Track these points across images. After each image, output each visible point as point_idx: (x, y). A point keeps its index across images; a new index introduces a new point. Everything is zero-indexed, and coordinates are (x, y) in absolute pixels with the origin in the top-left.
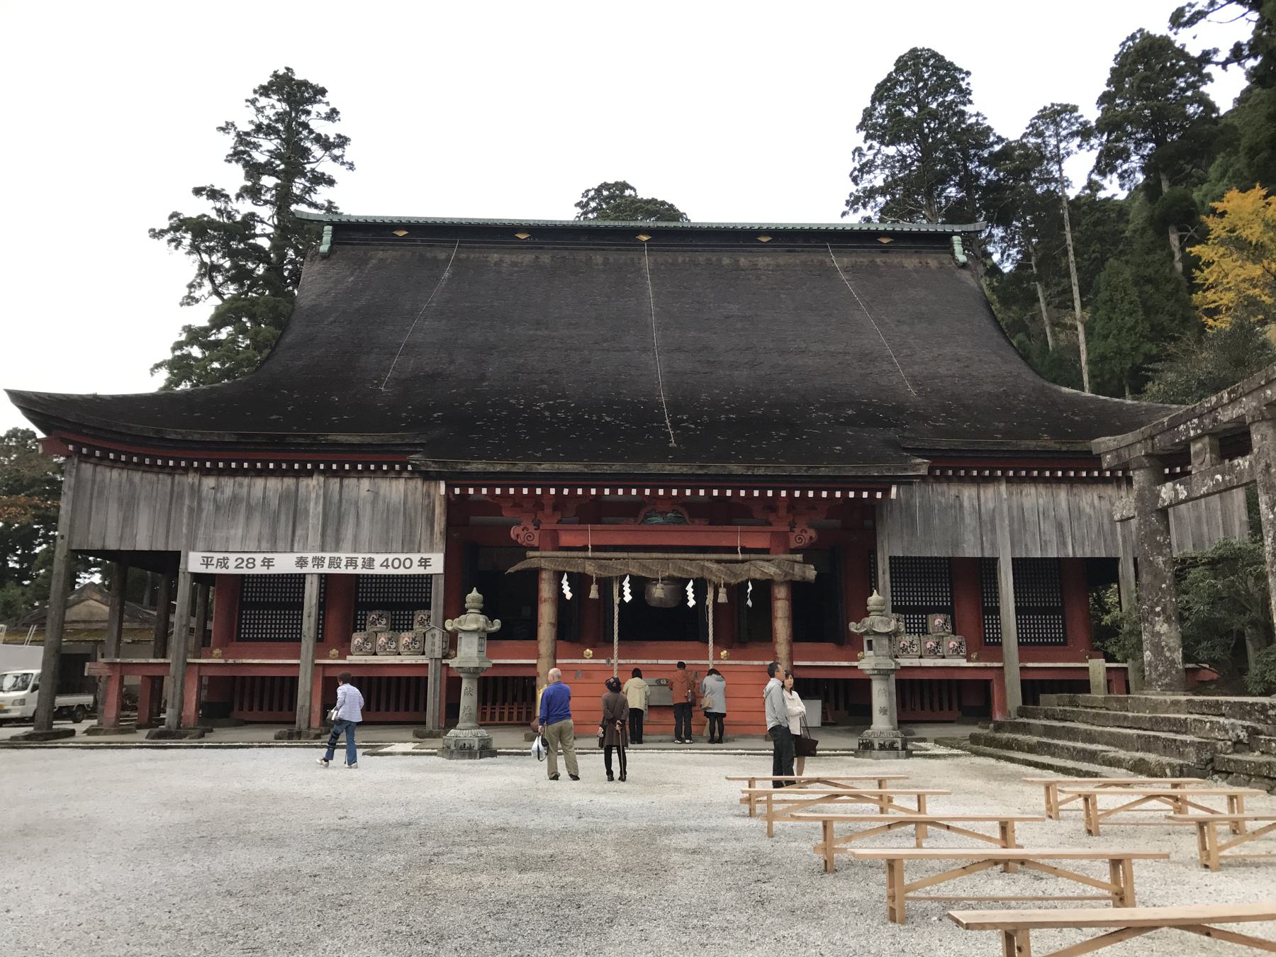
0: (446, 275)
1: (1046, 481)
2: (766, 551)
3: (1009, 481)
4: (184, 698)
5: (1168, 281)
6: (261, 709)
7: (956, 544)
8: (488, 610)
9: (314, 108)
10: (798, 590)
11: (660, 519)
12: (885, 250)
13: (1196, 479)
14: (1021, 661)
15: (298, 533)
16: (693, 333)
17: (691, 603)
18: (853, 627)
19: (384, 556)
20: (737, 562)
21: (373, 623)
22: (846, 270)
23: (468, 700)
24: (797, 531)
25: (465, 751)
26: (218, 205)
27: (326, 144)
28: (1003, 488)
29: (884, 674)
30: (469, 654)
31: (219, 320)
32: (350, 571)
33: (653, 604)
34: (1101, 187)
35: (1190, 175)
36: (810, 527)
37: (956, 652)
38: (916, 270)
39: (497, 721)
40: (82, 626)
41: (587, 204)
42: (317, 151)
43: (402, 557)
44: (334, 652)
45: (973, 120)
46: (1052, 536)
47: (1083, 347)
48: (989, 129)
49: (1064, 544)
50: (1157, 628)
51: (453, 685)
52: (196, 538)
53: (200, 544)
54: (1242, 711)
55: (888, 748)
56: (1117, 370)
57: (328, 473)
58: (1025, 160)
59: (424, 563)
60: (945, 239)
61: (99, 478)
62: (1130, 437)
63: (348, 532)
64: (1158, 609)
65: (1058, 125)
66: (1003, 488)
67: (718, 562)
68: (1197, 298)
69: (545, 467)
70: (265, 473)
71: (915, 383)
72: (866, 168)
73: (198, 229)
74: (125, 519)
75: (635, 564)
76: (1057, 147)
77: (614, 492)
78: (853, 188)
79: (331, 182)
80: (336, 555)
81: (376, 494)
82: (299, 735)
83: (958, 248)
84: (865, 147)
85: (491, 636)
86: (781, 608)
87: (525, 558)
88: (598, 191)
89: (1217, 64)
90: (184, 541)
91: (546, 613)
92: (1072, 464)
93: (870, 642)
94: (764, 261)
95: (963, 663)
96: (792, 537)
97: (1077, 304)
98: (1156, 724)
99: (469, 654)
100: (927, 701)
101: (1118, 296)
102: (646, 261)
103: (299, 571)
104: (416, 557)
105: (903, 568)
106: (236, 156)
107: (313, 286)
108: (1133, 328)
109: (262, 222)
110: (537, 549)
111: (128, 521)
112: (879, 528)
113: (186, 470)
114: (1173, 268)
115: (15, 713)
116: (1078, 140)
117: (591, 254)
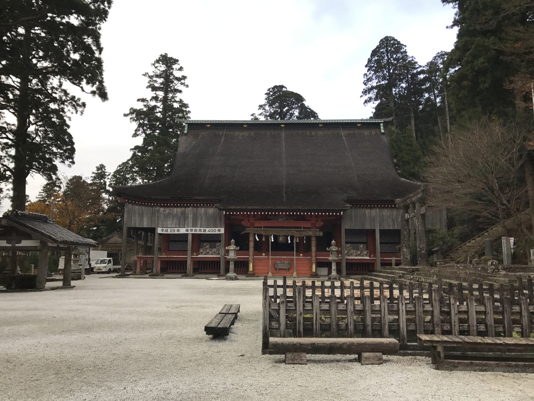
2: (310, 228)
3: (379, 208)
4: (157, 267)
8: (236, 244)
9: (174, 67)
10: (318, 238)
11: (281, 219)
12: (359, 128)
15: (186, 222)
17: (289, 242)
22: (345, 136)
23: (232, 266)
24: (318, 222)
25: (231, 279)
26: (145, 104)
30: (232, 255)
32: (200, 233)
37: (366, 255)
40: (113, 245)
41: (269, 93)
42: (176, 82)
43: (213, 229)
44: (195, 254)
45: (411, 59)
48: (416, 63)
49: (394, 225)
51: (227, 263)
53: (160, 225)
57: (194, 206)
59: (219, 230)
60: (379, 124)
63: (199, 222)
69: (250, 207)
72: (369, 80)
78: (365, 87)
79: (180, 91)
81: (206, 212)
82: (188, 276)
83: (382, 127)
86: (314, 243)
87: (245, 230)
88: (273, 88)
91: (251, 244)
92: (389, 204)
94: (320, 133)
96: (317, 224)
99: (232, 255)
100: (174, 267)
104: (217, 229)
105: (349, 232)
107: (184, 144)
109: (159, 107)
110: (248, 227)
111: (142, 220)
115: (104, 270)
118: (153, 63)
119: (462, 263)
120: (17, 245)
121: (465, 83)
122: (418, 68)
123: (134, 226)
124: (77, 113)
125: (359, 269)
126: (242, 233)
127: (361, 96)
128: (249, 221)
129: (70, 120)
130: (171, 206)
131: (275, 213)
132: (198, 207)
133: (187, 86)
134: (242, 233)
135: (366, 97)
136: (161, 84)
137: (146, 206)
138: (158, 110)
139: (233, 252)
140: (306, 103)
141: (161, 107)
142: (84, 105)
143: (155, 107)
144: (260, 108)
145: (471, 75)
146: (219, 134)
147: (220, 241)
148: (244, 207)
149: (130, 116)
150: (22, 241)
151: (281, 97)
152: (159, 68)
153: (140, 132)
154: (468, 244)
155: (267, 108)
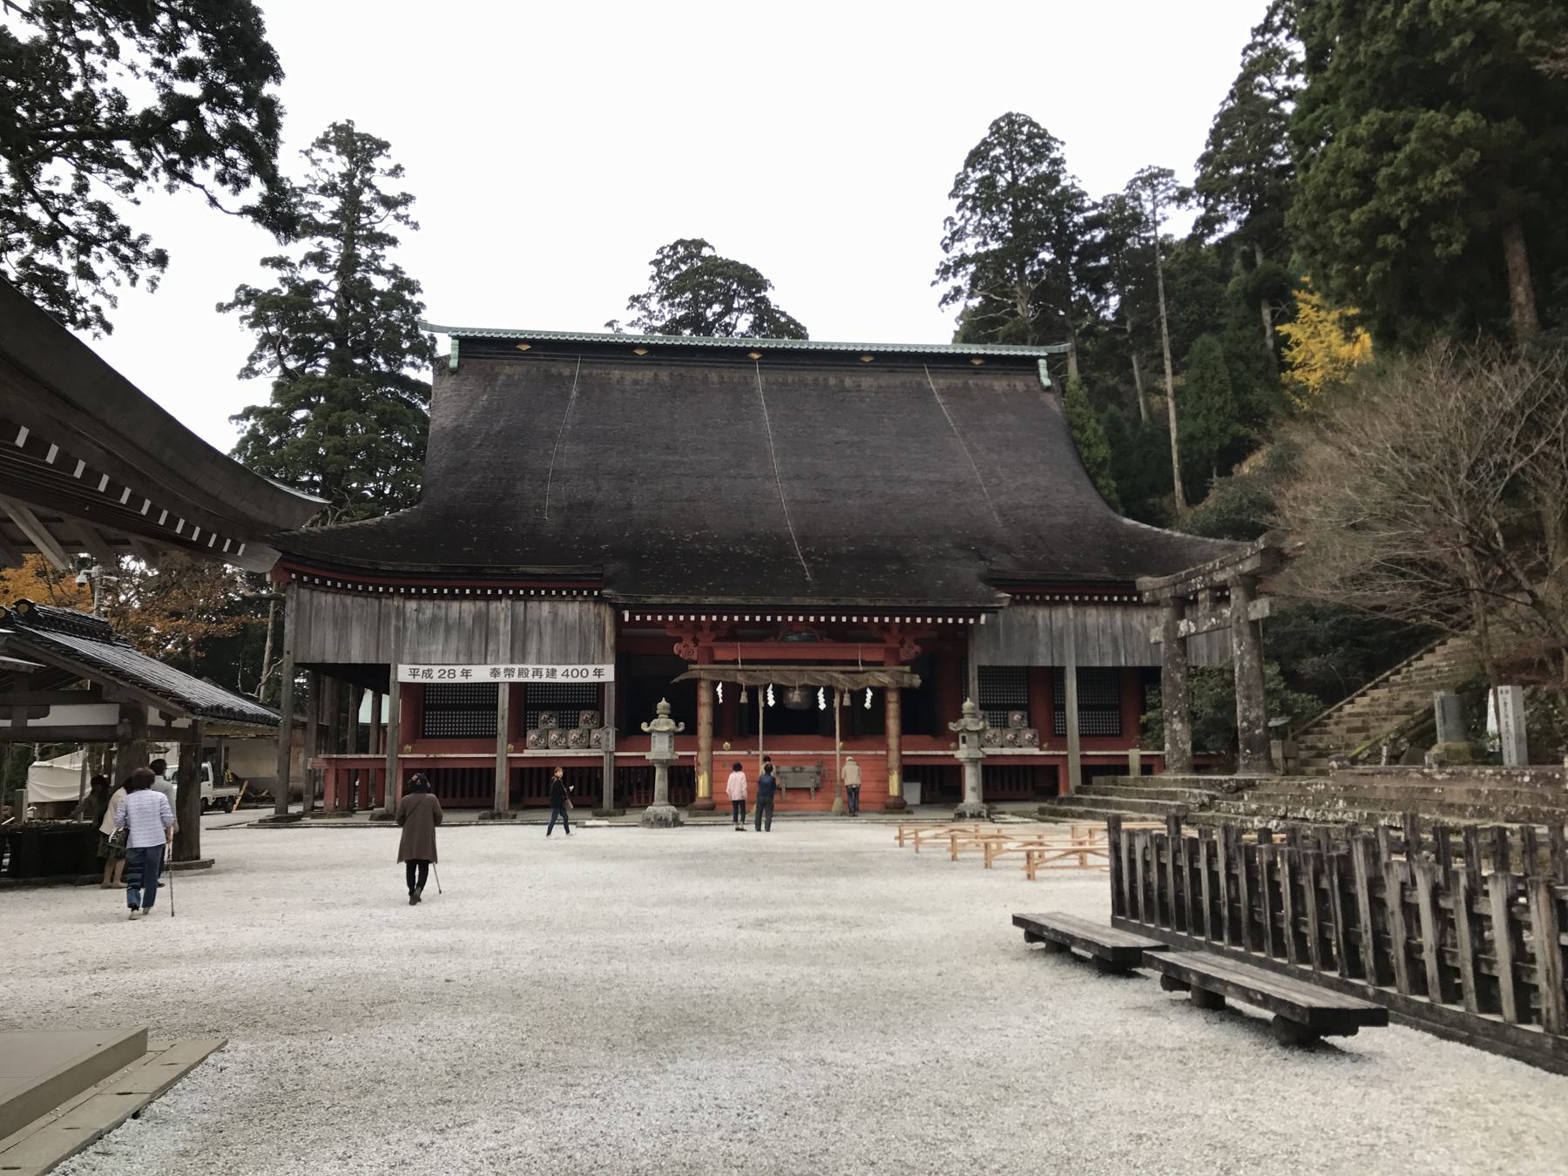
0: (574, 393)
1: (1105, 604)
2: (881, 664)
3: (1075, 604)
5: (1258, 358)
6: (463, 796)
7: (1032, 655)
10: (906, 694)
11: (795, 638)
12: (977, 371)
13: (1201, 621)
14: (1082, 748)
15: (491, 647)
16: (808, 460)
17: (822, 706)
18: (952, 726)
19: (564, 668)
20: (858, 672)
21: (545, 722)
22: (941, 392)
25: (662, 822)
26: (286, 273)
28: (1070, 610)
29: (974, 761)
32: (537, 679)
37: (1031, 743)
38: (1005, 394)
41: (661, 261)
42: (380, 210)
43: (580, 668)
46: (1108, 648)
47: (1173, 425)
48: (1083, 194)
53: (407, 658)
54: (1211, 785)
55: (977, 816)
56: (1205, 451)
58: (1123, 218)
59: (598, 673)
60: (1032, 362)
61: (315, 601)
63: (533, 647)
65: (1153, 187)
66: (1070, 610)
67: (843, 672)
68: (1285, 377)
69: (711, 600)
70: (462, 597)
71: (1001, 513)
72: (958, 235)
74: (340, 637)
75: (777, 675)
76: (1154, 212)
79: (393, 242)
83: (1043, 371)
84: (957, 217)
86: (893, 709)
92: (1121, 593)
94: (867, 382)
95: (1036, 751)
97: (1168, 370)
98: (1159, 795)
101: (1208, 375)
102: (759, 380)
103: (493, 680)
104: (591, 668)
108: (1222, 408)
110: (695, 663)
111: (342, 639)
113: (392, 595)
114: (1264, 345)
117: (706, 371)
118: (308, 147)
119: (1364, 762)
120: (31, 723)
121: (1389, 240)
122: (1088, 209)
123: (318, 660)
124: (133, 283)
126: (676, 680)
127: (934, 283)
128: (696, 641)
129: (114, 306)
130: (441, 596)
131: (763, 619)
132: (530, 598)
133: (416, 226)
134: (676, 680)
135: (946, 287)
136: (335, 215)
137: (357, 594)
138: (323, 296)
139: (666, 738)
140: (775, 297)
141: (335, 286)
142: (160, 259)
143: (315, 286)
144: (632, 306)
145: (1406, 217)
146: (560, 374)
148: (691, 600)
149: (237, 312)
150: (53, 709)
151: (700, 277)
152: (324, 165)
154: (1348, 709)
155: (653, 304)
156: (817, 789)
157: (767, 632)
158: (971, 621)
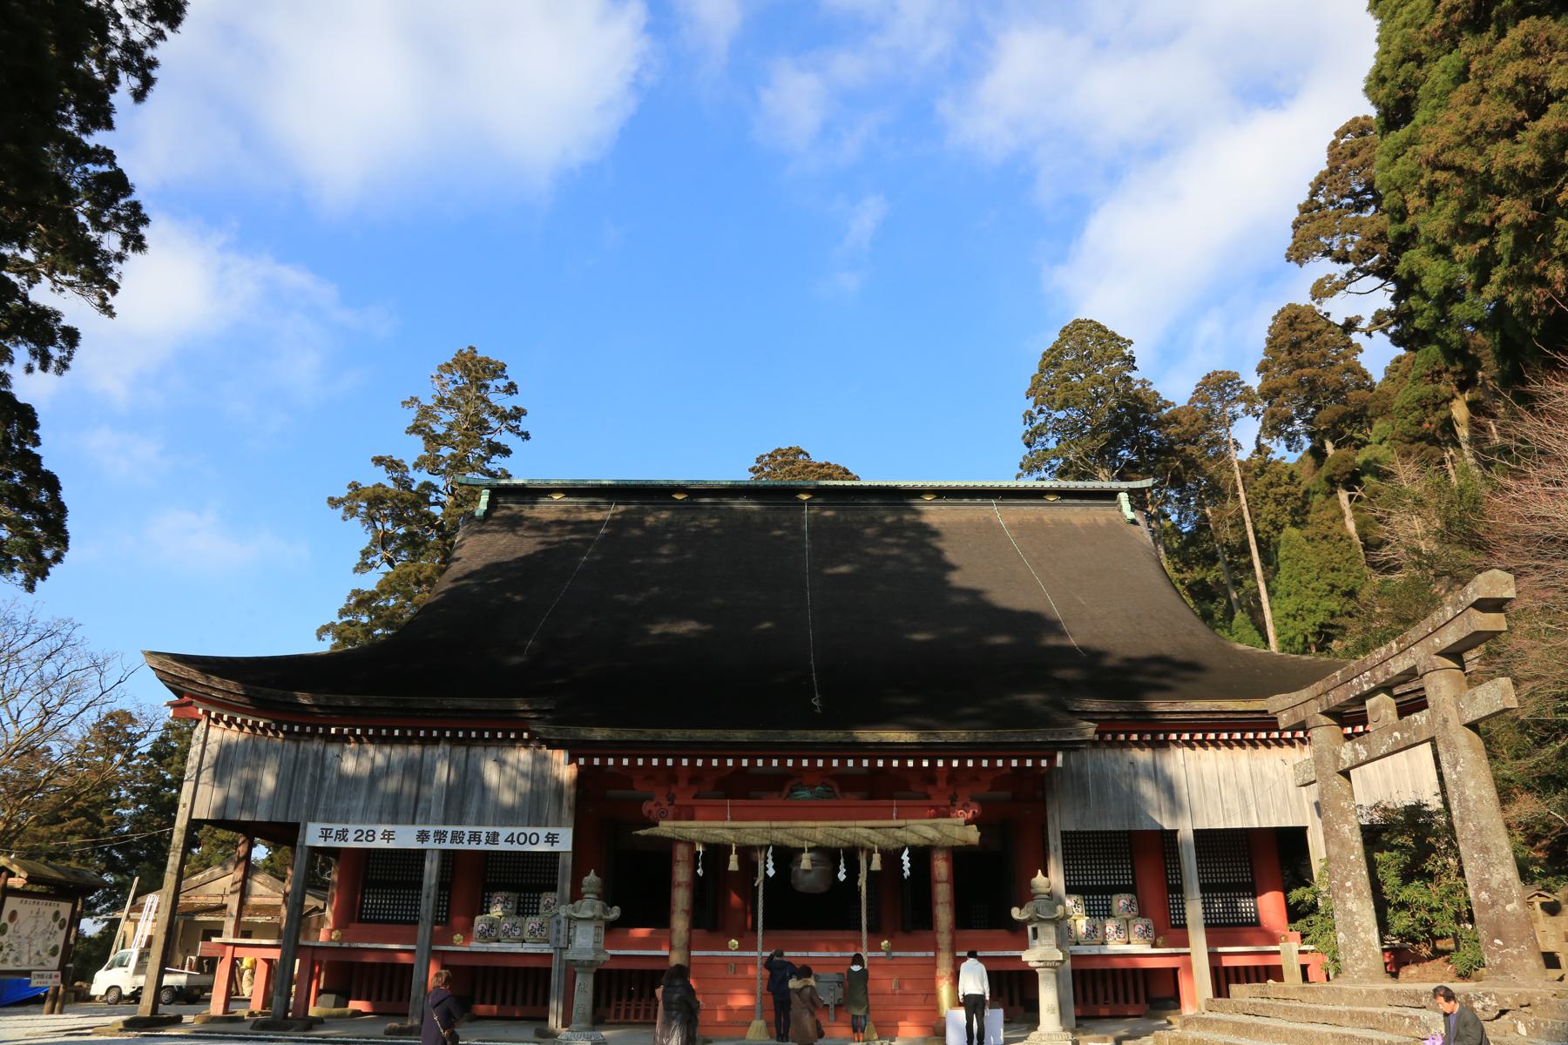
11: (806, 794)
27: (504, 417)
30: (585, 943)
31: (387, 587)
32: (473, 846)
33: (801, 888)
34: (1270, 451)
35: (1352, 439)
36: (973, 800)
39: (622, 1018)
42: (494, 423)
43: (528, 831)
45: (1138, 386)
49: (1248, 813)
50: (1349, 905)
52: (316, 808)
57: (454, 741)
59: (551, 839)
60: (1111, 495)
62: (1305, 694)
64: (1348, 884)
72: (1038, 432)
73: (376, 499)
77: (843, 763)
79: (506, 452)
80: (459, 828)
85: (611, 926)
89: (1362, 331)
90: (304, 812)
93: (1035, 930)
99: (585, 943)
103: (417, 845)
104: (543, 832)
106: (415, 429)
112: (1049, 800)
113: (312, 736)
116: (1242, 405)
125: (1101, 996)
133: (526, 436)
147: (553, 888)
153: (377, 559)
156: (838, 1006)
157: (778, 783)
158: (1044, 763)
